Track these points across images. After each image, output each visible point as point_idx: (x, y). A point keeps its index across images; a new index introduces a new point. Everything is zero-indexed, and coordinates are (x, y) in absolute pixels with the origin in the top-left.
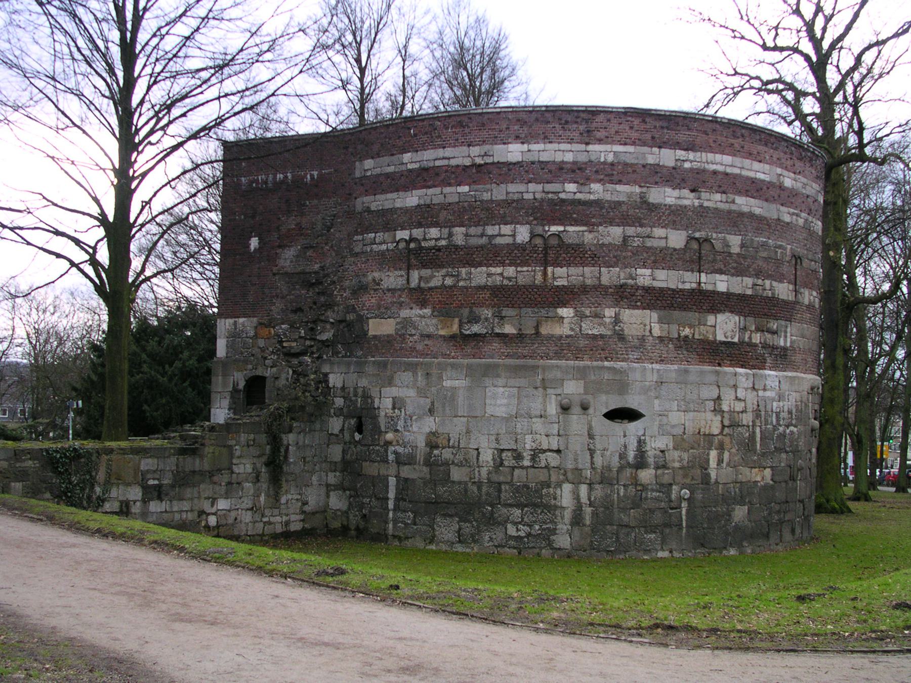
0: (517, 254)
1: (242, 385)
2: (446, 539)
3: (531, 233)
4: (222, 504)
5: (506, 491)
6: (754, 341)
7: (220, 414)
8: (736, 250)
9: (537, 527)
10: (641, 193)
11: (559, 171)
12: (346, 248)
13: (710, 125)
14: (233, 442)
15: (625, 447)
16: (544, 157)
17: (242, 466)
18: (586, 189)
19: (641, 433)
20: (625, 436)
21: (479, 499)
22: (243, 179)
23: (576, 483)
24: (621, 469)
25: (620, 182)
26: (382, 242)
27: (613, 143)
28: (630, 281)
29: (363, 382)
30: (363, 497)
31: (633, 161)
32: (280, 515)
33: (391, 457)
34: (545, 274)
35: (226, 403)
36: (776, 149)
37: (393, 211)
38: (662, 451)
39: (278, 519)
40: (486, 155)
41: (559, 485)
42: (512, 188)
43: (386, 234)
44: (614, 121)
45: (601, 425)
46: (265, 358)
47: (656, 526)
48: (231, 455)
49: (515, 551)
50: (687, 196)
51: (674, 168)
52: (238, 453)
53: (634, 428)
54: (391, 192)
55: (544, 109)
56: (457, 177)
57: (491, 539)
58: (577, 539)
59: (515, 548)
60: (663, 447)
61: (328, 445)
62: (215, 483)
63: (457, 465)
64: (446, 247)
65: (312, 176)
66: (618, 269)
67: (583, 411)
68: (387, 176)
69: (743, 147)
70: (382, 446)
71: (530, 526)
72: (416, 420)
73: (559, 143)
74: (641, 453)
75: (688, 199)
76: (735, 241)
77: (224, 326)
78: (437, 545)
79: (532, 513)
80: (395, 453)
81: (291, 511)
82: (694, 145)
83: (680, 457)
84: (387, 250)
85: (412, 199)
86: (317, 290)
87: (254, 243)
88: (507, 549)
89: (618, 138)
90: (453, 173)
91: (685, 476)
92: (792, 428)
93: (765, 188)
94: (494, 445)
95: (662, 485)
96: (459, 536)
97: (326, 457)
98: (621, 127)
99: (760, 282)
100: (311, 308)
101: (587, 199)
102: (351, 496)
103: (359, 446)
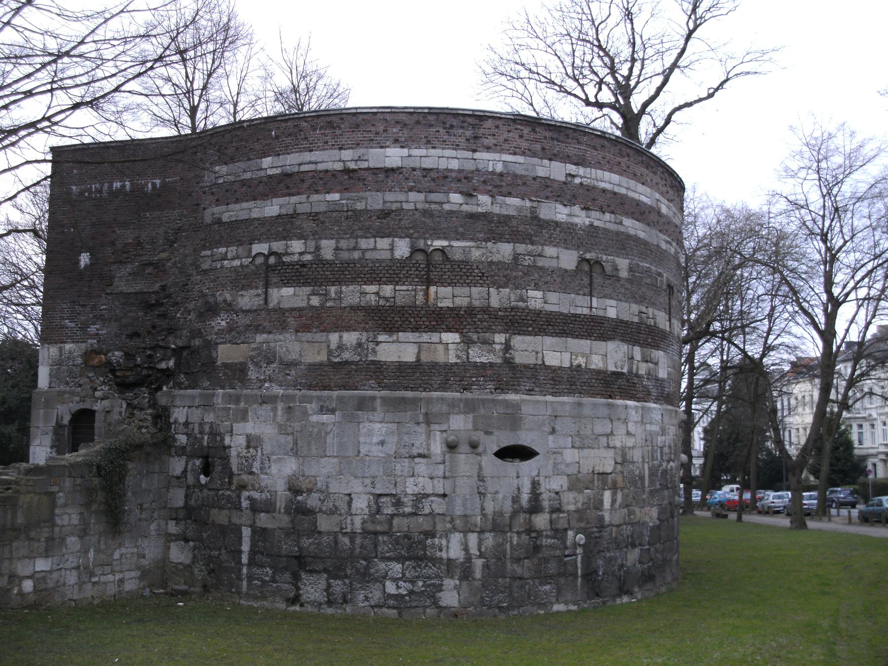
0: (391, 271)
1: (66, 420)
2: (312, 598)
3: (412, 247)
4: (42, 565)
5: (384, 542)
6: (640, 372)
7: (40, 452)
8: (624, 274)
9: (420, 583)
10: (532, 207)
11: (438, 179)
12: (191, 265)
13: (598, 140)
14: (55, 489)
15: (519, 489)
16: (428, 164)
17: (66, 517)
18: (474, 200)
19: (534, 473)
20: (518, 477)
21: (352, 552)
22: (74, 187)
23: (465, 532)
24: (515, 514)
25: (509, 194)
26: (232, 258)
27: (501, 151)
28: (520, 304)
29: (210, 418)
30: (211, 550)
31: (523, 173)
32: (113, 572)
33: (245, 504)
34: (427, 294)
35: (48, 440)
36: (655, 173)
37: (249, 221)
38: (557, 493)
39: (110, 577)
40: (360, 159)
41: (446, 534)
42: (390, 197)
43: (240, 249)
44: (504, 128)
45: (490, 463)
46: (95, 389)
47: (551, 577)
48: (53, 505)
49: (395, 611)
50: (577, 213)
51: (565, 183)
52: (61, 501)
53: (528, 468)
54: (247, 201)
55: (426, 111)
56: (325, 184)
57: (367, 598)
58: (467, 595)
59: (394, 608)
60: (558, 488)
61: (168, 489)
62: (32, 539)
63: (324, 513)
64: (311, 263)
65: (154, 184)
66: (508, 290)
67: (472, 450)
68: (243, 183)
69: (628, 167)
70: (233, 491)
71: (413, 582)
72: (275, 461)
73: (443, 149)
74: (535, 495)
75: (581, 218)
76: (623, 264)
77: (47, 354)
78: (302, 605)
79: (414, 568)
80: (250, 498)
81: (125, 567)
82: (584, 160)
83: (575, 498)
84: (242, 266)
85: (272, 208)
86: (157, 313)
87: (84, 259)
88: (385, 610)
89: (506, 146)
90: (321, 179)
91: (580, 520)
92: (671, 463)
93: (647, 212)
94: (369, 489)
95: (556, 530)
96: (329, 595)
97: (166, 502)
98: (511, 135)
99: (644, 309)
100: (149, 332)
101: (475, 211)
102: (195, 548)
103: (205, 490)
